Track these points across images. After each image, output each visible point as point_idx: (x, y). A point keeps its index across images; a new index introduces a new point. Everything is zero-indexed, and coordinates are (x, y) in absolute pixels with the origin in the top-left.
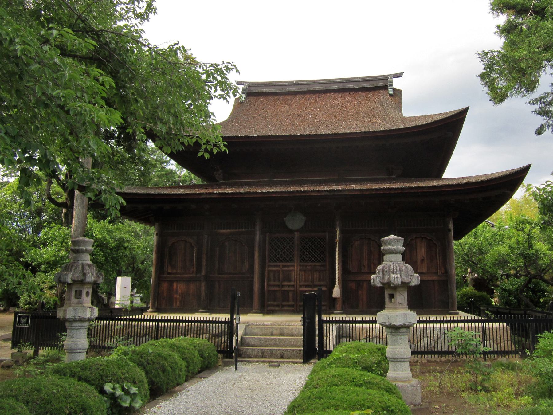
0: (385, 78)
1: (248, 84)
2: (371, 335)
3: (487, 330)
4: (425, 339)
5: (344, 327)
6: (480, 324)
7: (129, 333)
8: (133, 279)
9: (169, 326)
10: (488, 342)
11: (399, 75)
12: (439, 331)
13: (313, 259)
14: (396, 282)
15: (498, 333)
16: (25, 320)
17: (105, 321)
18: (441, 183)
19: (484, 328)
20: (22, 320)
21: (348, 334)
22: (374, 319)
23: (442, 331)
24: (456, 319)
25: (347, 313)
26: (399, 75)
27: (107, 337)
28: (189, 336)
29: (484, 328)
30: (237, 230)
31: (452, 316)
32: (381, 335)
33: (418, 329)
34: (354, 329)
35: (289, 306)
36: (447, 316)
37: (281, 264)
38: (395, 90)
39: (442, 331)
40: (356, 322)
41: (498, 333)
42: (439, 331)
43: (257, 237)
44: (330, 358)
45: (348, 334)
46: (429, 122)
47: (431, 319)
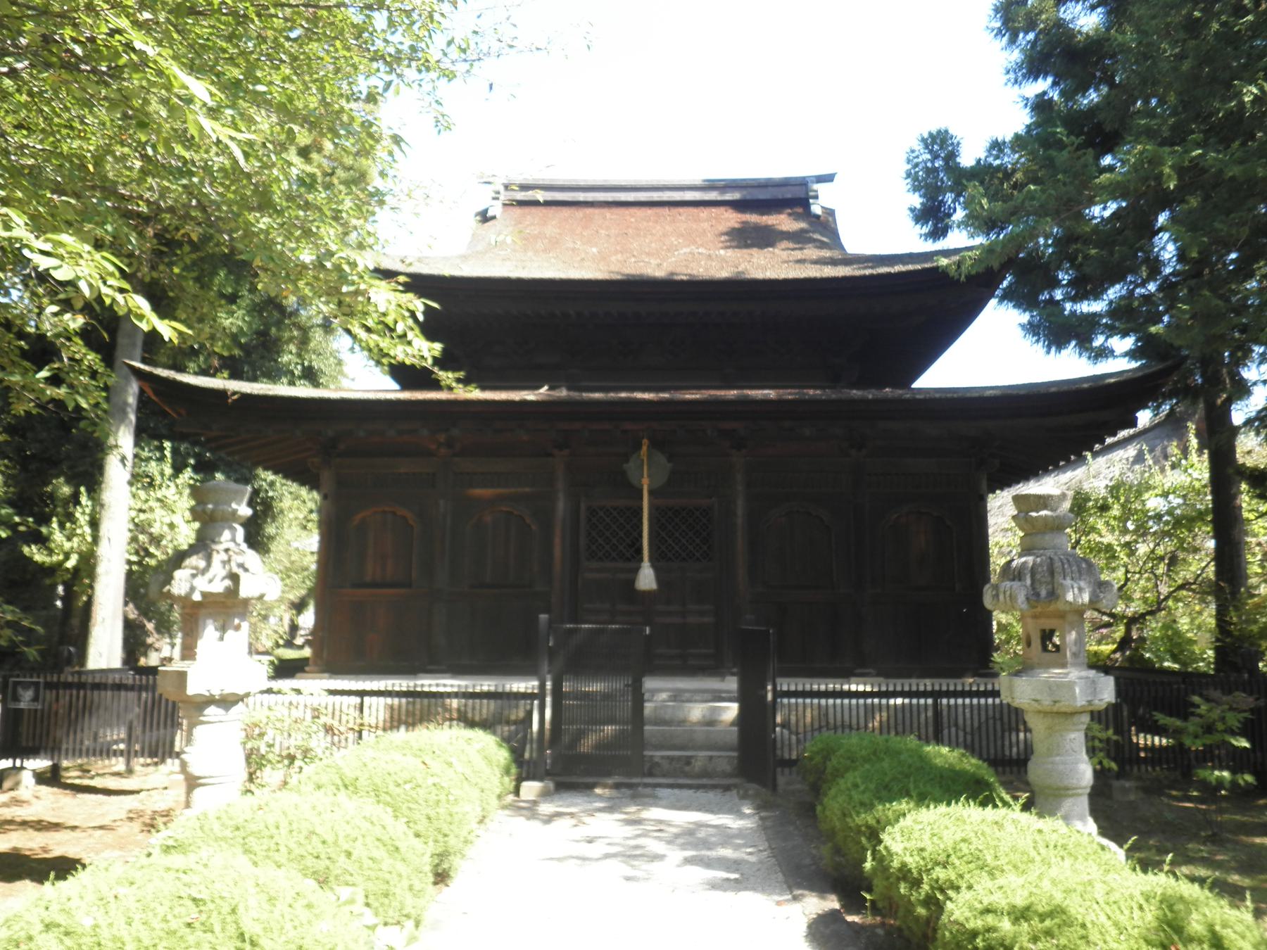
0: (803, 183)
2: (831, 721)
3: (945, 713)
4: (953, 730)
6: (930, 701)
7: (979, 727)
8: (632, 582)
10: (946, 732)
11: (828, 178)
12: (983, 713)
13: (614, 554)
20: (20, 691)
21: (839, 723)
22: (990, 687)
23: (991, 713)
24: (959, 688)
25: (887, 674)
26: (828, 178)
27: (999, 734)
28: (893, 733)
30: (512, 490)
32: (854, 721)
33: (915, 709)
34: (854, 708)
39: (991, 713)
40: (819, 694)
42: (983, 713)
43: (561, 506)
45: (839, 723)
46: (660, 273)
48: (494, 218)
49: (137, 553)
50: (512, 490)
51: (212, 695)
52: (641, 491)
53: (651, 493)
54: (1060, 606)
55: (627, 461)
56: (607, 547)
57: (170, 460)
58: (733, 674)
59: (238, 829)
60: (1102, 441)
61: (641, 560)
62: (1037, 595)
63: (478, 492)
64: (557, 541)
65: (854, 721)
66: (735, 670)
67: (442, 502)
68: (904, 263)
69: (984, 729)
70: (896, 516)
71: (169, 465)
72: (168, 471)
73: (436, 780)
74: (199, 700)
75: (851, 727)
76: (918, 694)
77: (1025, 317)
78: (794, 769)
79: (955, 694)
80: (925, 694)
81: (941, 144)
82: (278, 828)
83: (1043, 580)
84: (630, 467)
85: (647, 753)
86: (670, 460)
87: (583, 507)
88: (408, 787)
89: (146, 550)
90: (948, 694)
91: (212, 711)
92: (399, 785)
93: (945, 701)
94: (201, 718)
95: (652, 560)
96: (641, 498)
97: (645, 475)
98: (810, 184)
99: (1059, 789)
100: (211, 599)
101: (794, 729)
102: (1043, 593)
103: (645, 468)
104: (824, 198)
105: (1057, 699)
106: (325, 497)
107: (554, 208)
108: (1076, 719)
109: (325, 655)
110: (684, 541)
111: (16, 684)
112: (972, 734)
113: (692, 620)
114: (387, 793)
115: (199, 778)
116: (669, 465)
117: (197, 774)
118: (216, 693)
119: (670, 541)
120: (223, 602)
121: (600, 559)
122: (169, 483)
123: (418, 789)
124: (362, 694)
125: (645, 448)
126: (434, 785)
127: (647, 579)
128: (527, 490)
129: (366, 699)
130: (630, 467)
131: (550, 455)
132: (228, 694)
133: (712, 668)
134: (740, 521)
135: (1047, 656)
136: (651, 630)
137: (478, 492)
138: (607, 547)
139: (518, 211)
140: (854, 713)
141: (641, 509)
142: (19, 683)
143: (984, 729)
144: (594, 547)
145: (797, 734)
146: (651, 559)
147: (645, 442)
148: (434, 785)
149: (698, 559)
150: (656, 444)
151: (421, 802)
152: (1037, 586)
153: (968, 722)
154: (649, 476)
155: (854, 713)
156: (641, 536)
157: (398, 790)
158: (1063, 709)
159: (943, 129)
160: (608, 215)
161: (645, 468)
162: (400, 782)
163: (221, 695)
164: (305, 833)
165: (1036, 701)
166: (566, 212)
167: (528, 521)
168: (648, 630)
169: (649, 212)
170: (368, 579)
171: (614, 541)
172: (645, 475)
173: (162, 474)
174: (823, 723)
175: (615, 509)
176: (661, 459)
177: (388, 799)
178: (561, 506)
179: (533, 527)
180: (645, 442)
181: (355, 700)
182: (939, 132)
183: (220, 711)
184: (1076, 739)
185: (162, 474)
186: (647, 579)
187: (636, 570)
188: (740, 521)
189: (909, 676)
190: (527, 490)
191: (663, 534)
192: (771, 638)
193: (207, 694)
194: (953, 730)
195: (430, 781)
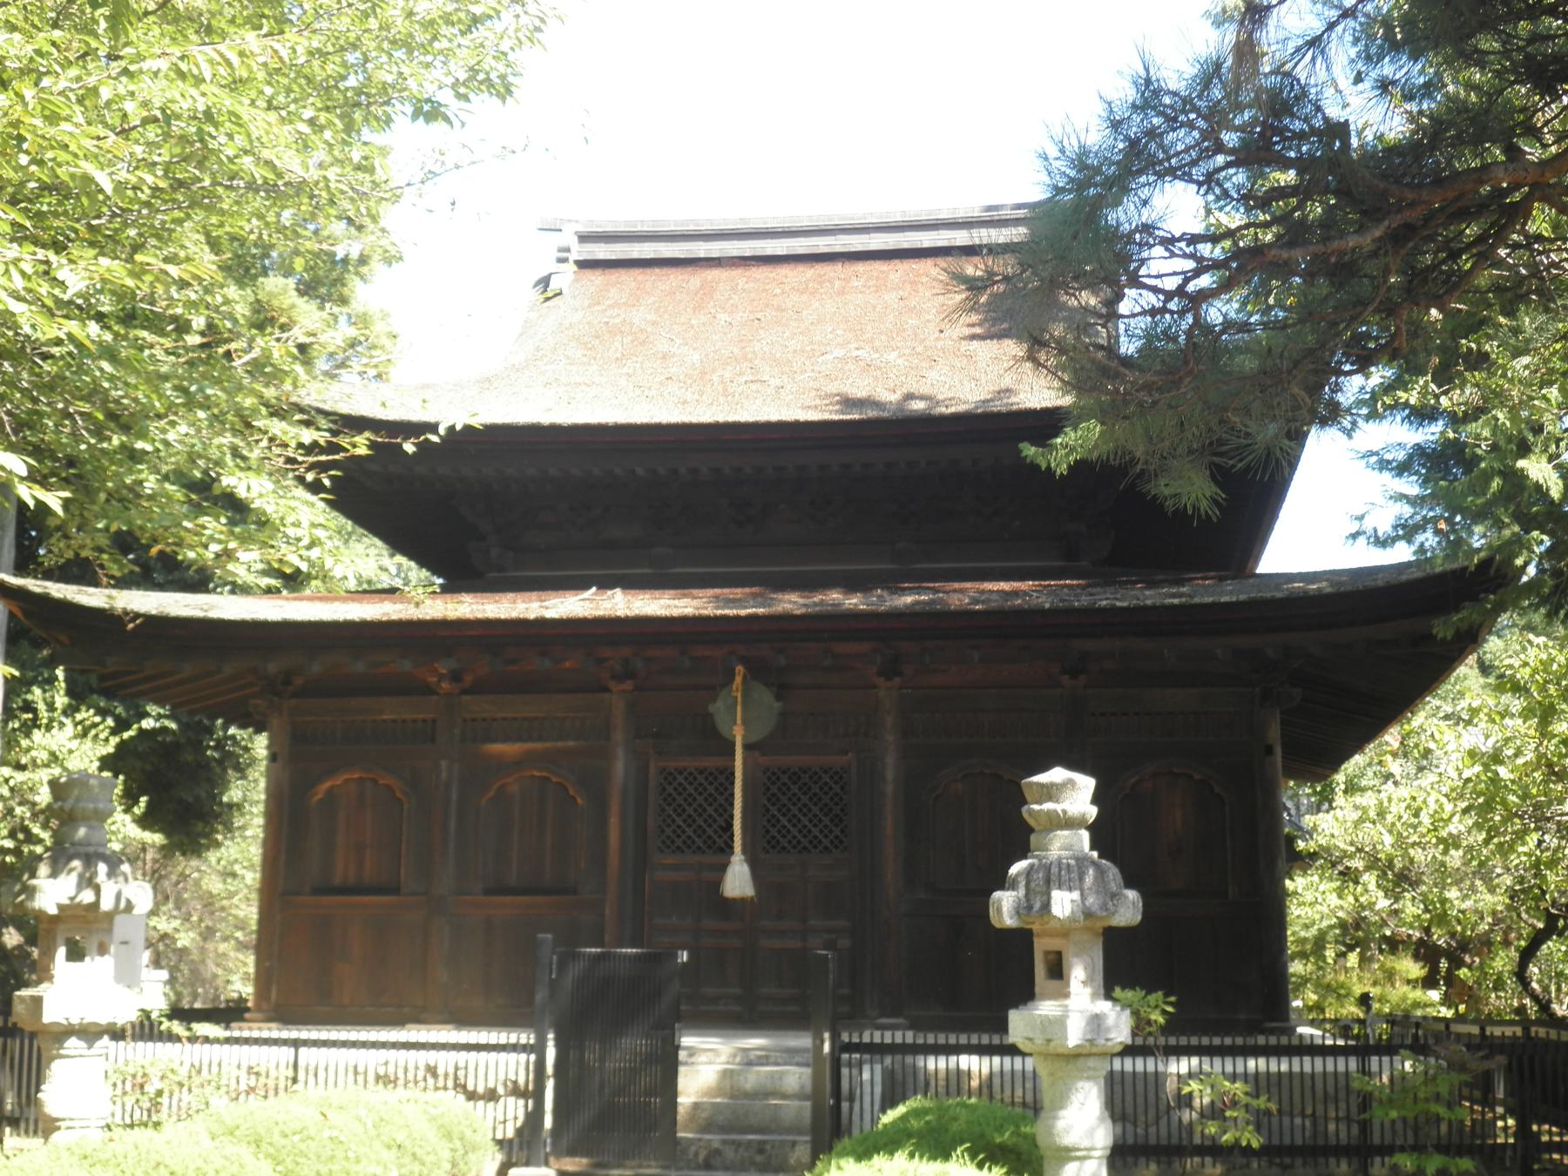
8: (718, 883)
13: (805, 842)
25: (915, 1026)
43: (620, 767)
49: (12, 835)
50: (548, 745)
51: (70, 1024)
52: (733, 744)
53: (748, 747)
57: (63, 685)
59: (86, 1157)
62: (1030, 908)
64: (614, 822)
67: (444, 764)
70: (1133, 781)
71: (62, 692)
72: (61, 700)
73: (335, 1133)
74: (56, 1029)
77: (458, 428)
82: (126, 1157)
83: (1038, 889)
84: (718, 708)
85: (680, 1134)
86: (778, 698)
87: (652, 770)
88: (296, 1138)
89: (26, 830)
91: (73, 1043)
92: (286, 1136)
94: (62, 1052)
96: (732, 754)
97: (739, 721)
100: (69, 913)
102: (1037, 906)
103: (739, 709)
105: (1049, 1037)
107: (657, 270)
109: (273, 996)
110: (690, 832)
114: (271, 1144)
115: (58, 1120)
116: (777, 705)
117: (55, 1115)
118: (75, 1021)
120: (84, 917)
122: (63, 719)
123: (309, 1141)
124: (296, 1044)
125: (738, 680)
126: (331, 1138)
127: (738, 880)
128: (571, 743)
129: (302, 1050)
130: (718, 708)
131: (606, 690)
132: (90, 1024)
134: (889, 789)
136: (690, 956)
139: (596, 278)
144: (679, 842)
146: (744, 851)
147: (740, 669)
148: (331, 1138)
149: (826, 848)
151: (311, 1156)
152: (1032, 897)
154: (744, 722)
157: (283, 1141)
160: (741, 282)
161: (739, 709)
162: (288, 1132)
163: (80, 1024)
164: (153, 1163)
165: (1030, 1039)
166: (675, 277)
167: (572, 792)
170: (337, 881)
172: (739, 721)
173: (51, 707)
175: (701, 772)
177: (271, 1150)
178: (620, 767)
179: (579, 801)
180: (740, 669)
181: (287, 1053)
183: (82, 1044)
185: (51, 707)
186: (738, 880)
187: (723, 867)
188: (889, 789)
190: (571, 743)
191: (774, 810)
192: (831, 965)
193: (65, 1022)
195: (327, 1134)
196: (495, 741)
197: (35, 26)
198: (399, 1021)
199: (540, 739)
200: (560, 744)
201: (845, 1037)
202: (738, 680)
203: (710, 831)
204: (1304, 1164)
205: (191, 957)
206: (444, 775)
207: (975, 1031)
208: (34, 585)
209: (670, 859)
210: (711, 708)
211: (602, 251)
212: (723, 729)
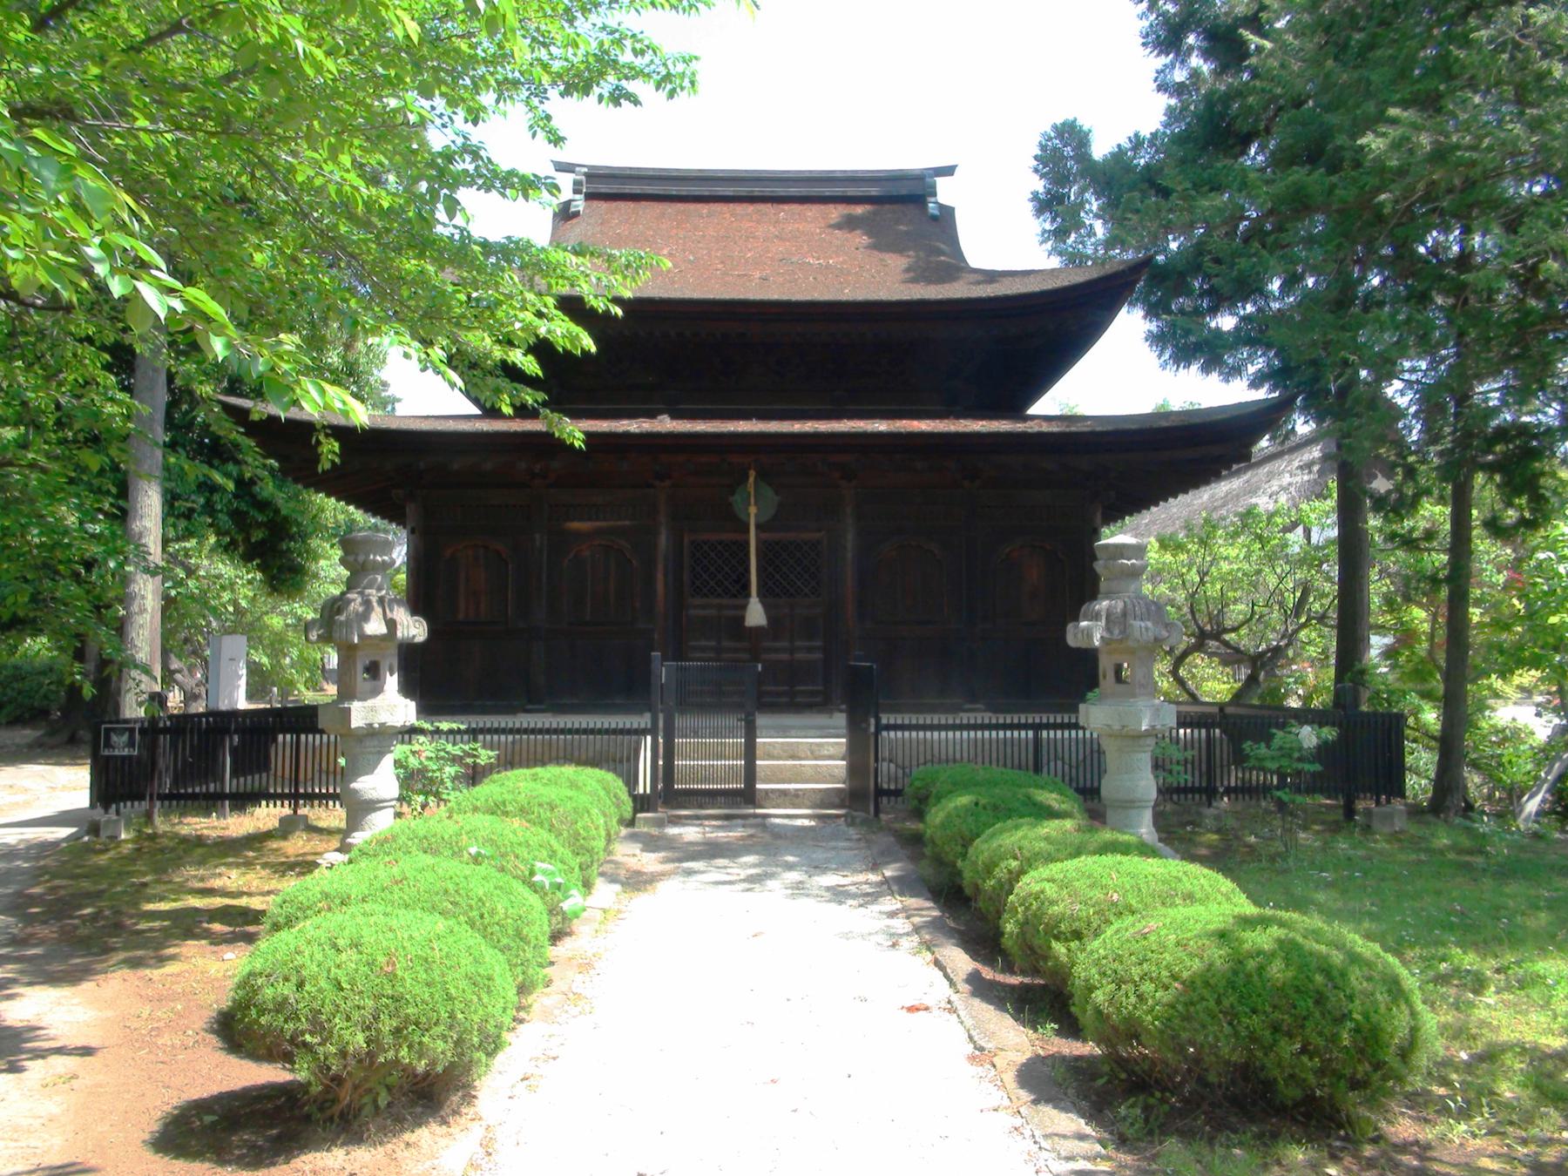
1: (586, 170)
3: (1045, 743)
4: (1059, 763)
5: (554, 742)
6: (1031, 734)
8: (743, 618)
9: (958, 741)
11: (948, 171)
13: (719, 590)
14: (1145, 637)
15: (1073, 749)
16: (125, 738)
17: (1188, 731)
18: (1019, 427)
19: (1037, 741)
21: (951, 757)
25: (996, 710)
26: (948, 171)
29: (1037, 741)
30: (611, 523)
31: (972, 715)
32: (958, 756)
34: (958, 741)
35: (813, 694)
36: (962, 714)
37: (717, 601)
38: (942, 207)
41: (1073, 749)
43: (663, 540)
44: (1468, 823)
45: (951, 757)
47: (914, 722)
48: (576, 214)
50: (611, 523)
53: (758, 527)
54: (1131, 643)
55: (733, 493)
56: (712, 583)
58: (841, 711)
60: (1230, 467)
61: (748, 595)
63: (576, 525)
64: (660, 577)
65: (958, 756)
66: (844, 707)
67: (537, 536)
68: (784, 793)
69: (1088, 762)
75: (955, 761)
76: (1019, 727)
77: (1153, 326)
78: (900, 799)
79: (1055, 726)
80: (1026, 727)
81: (1071, 135)
84: (737, 499)
85: (758, 786)
86: (777, 493)
87: (686, 540)
90: (1048, 727)
93: (1045, 733)
95: (761, 595)
96: (747, 531)
98: (928, 180)
99: (1133, 801)
101: (900, 762)
104: (946, 191)
106: (412, 531)
108: (1142, 742)
111: (108, 731)
112: (1077, 768)
113: (799, 656)
119: (778, 577)
121: (706, 595)
125: (751, 480)
127: (756, 614)
128: (627, 523)
133: (818, 703)
134: (849, 555)
135: (1121, 687)
137: (576, 525)
138: (712, 583)
139: (603, 206)
140: (958, 747)
141: (747, 543)
142: (113, 730)
143: (1088, 762)
144: (705, 590)
145: (903, 768)
146: (758, 595)
147: (752, 474)
150: (763, 476)
153: (1074, 755)
155: (958, 747)
156: (747, 570)
158: (1131, 733)
159: (1071, 118)
168: (760, 667)
169: (750, 208)
171: (712, 569)
174: (929, 757)
176: (769, 492)
178: (663, 540)
180: (752, 474)
182: (1063, 124)
184: (1144, 760)
186: (756, 614)
187: (744, 607)
188: (849, 555)
189: (1009, 711)
190: (627, 523)
194: (1059, 763)
196: (573, 520)
197: (248, 10)
198: (511, 710)
199: (605, 520)
200: (619, 523)
201: (884, 721)
202: (751, 480)
203: (726, 583)
204: (1251, 798)
205: (1105, 634)
206: (538, 543)
207: (1058, 712)
208: (233, 400)
209: (698, 601)
210: (731, 499)
211: (604, 188)
212: (742, 516)
